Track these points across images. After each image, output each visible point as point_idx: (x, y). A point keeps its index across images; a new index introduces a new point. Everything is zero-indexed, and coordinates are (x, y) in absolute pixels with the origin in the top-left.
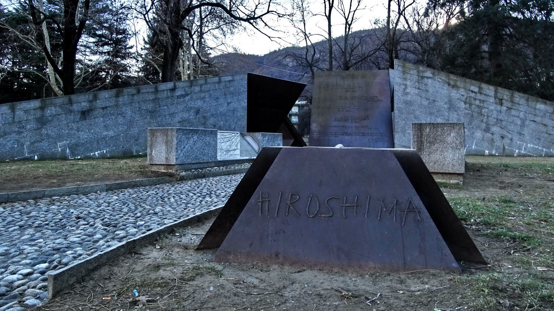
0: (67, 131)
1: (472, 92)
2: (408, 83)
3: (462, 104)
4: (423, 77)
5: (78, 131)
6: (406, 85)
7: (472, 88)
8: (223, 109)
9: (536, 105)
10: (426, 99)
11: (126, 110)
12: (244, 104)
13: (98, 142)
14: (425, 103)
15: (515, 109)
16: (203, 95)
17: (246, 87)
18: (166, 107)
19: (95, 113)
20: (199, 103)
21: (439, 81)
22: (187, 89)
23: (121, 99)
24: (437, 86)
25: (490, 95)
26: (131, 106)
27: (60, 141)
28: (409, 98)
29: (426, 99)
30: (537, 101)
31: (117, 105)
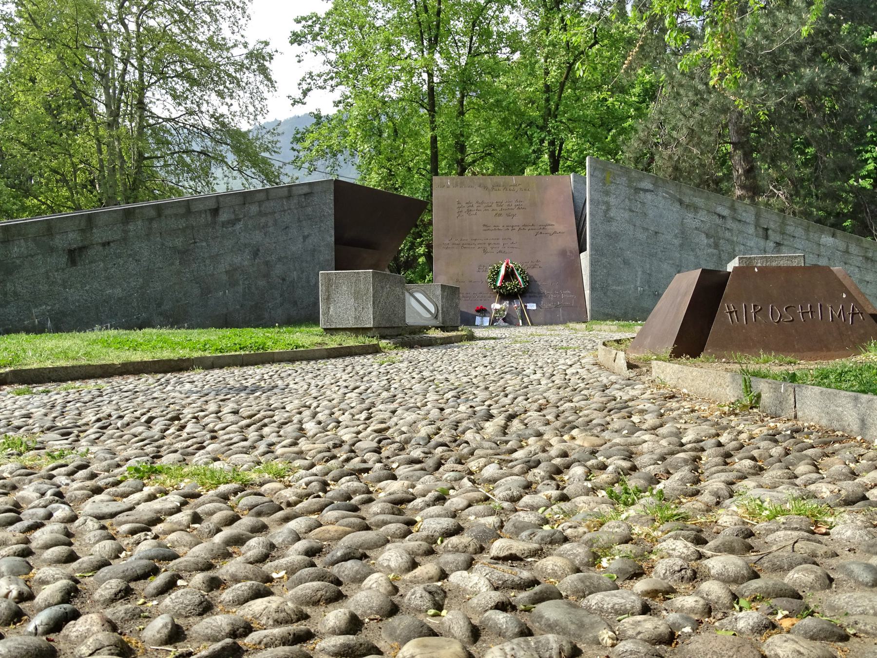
0: (46, 288)
1: (719, 215)
2: (612, 200)
3: (703, 236)
4: (637, 190)
5: (65, 288)
6: (607, 203)
7: (720, 209)
8: (296, 247)
9: (820, 238)
10: (643, 228)
11: (140, 248)
12: (329, 239)
13: (97, 308)
14: (642, 236)
15: (787, 246)
16: (263, 220)
17: (332, 206)
18: (204, 244)
19: (91, 252)
20: (258, 237)
21: (664, 197)
22: (237, 208)
23: (131, 227)
24: (661, 206)
25: (748, 221)
26: (149, 240)
27: (36, 307)
28: (614, 227)
29: (643, 228)
30: (822, 232)
31: (125, 240)
